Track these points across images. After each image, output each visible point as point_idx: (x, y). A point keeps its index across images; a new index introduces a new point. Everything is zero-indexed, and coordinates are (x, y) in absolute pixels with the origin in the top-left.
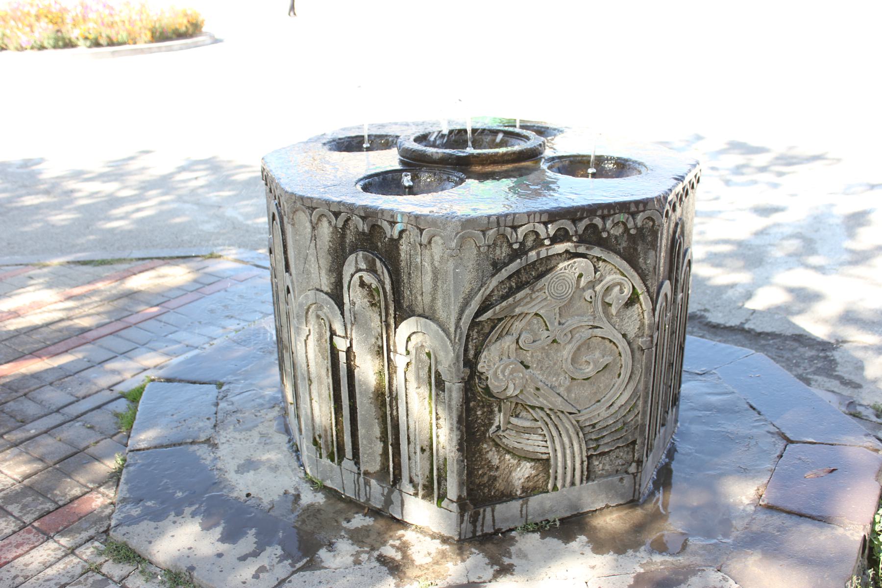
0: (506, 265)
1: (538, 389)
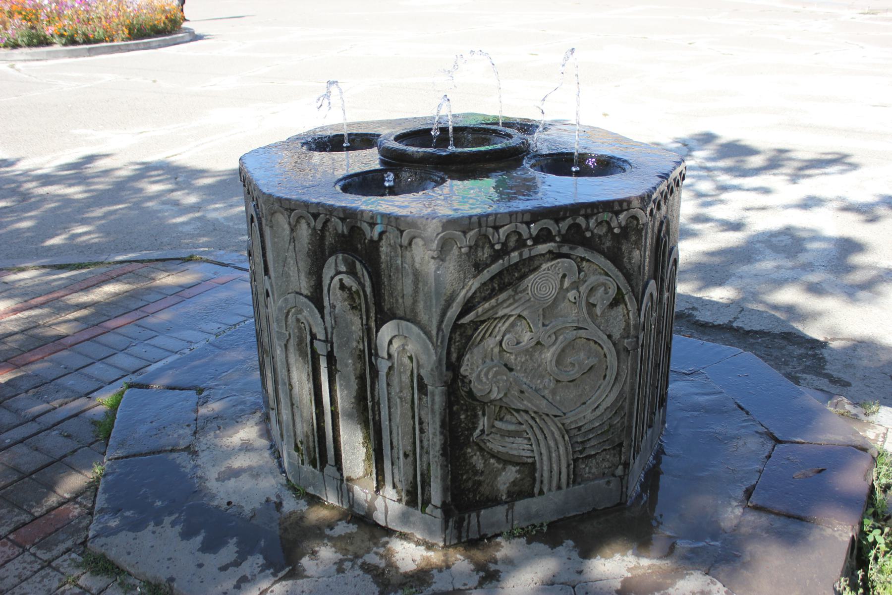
0: (488, 266)
1: (522, 392)
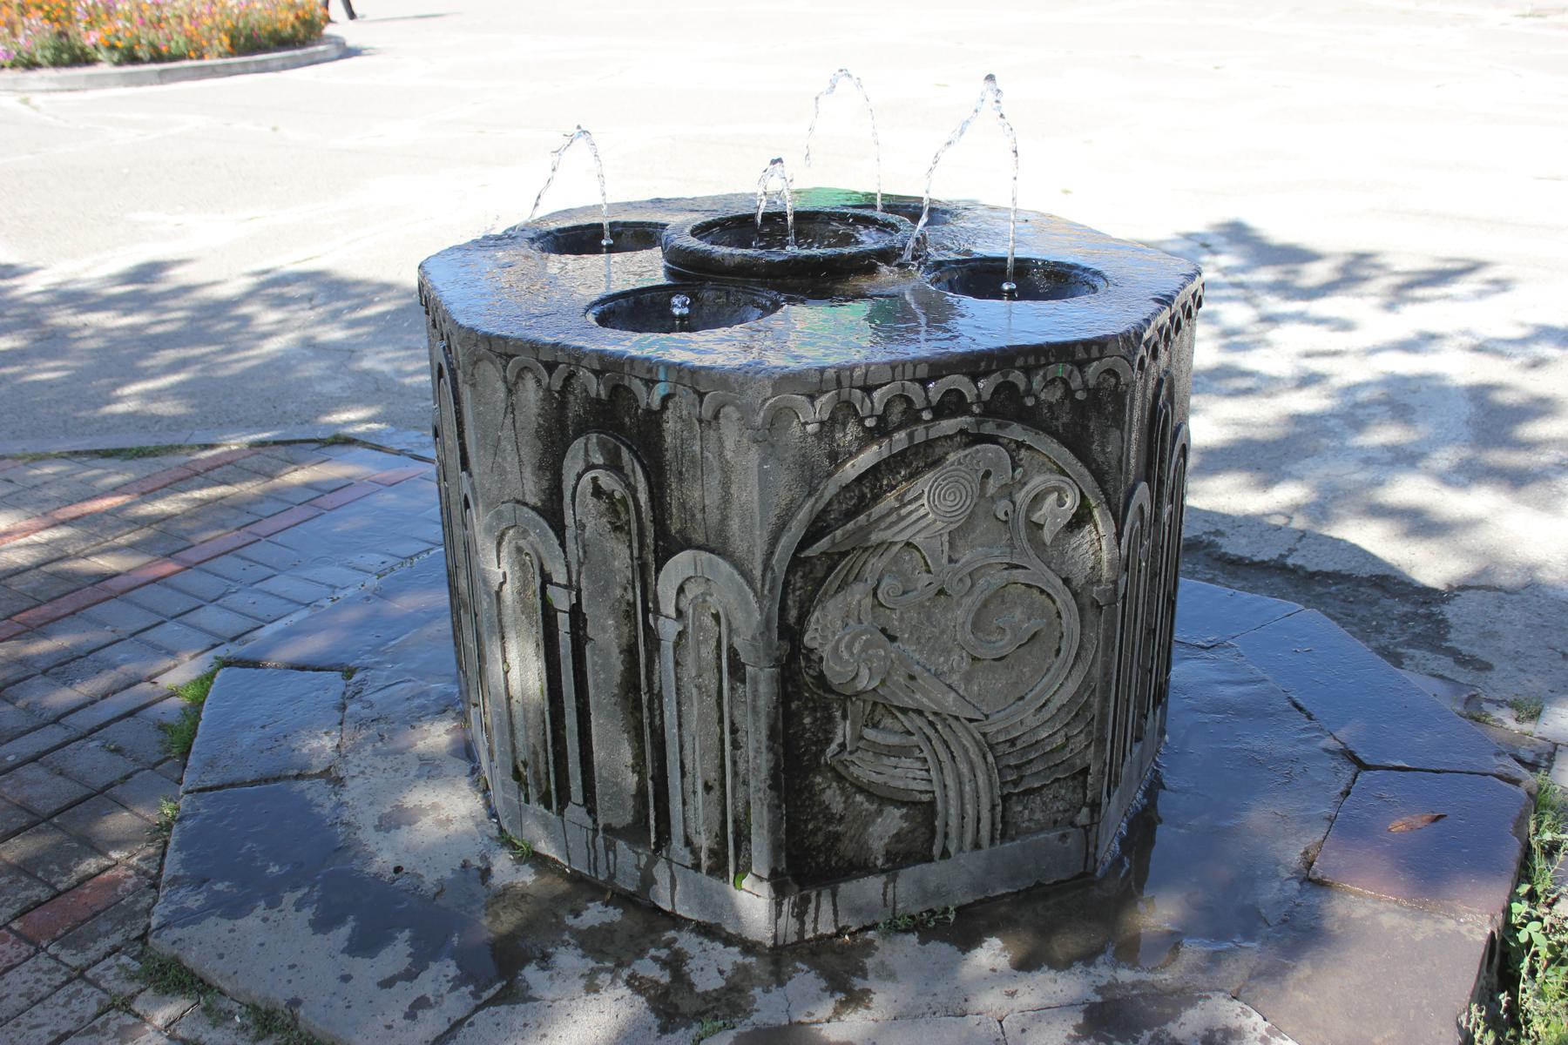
1: (912, 678)
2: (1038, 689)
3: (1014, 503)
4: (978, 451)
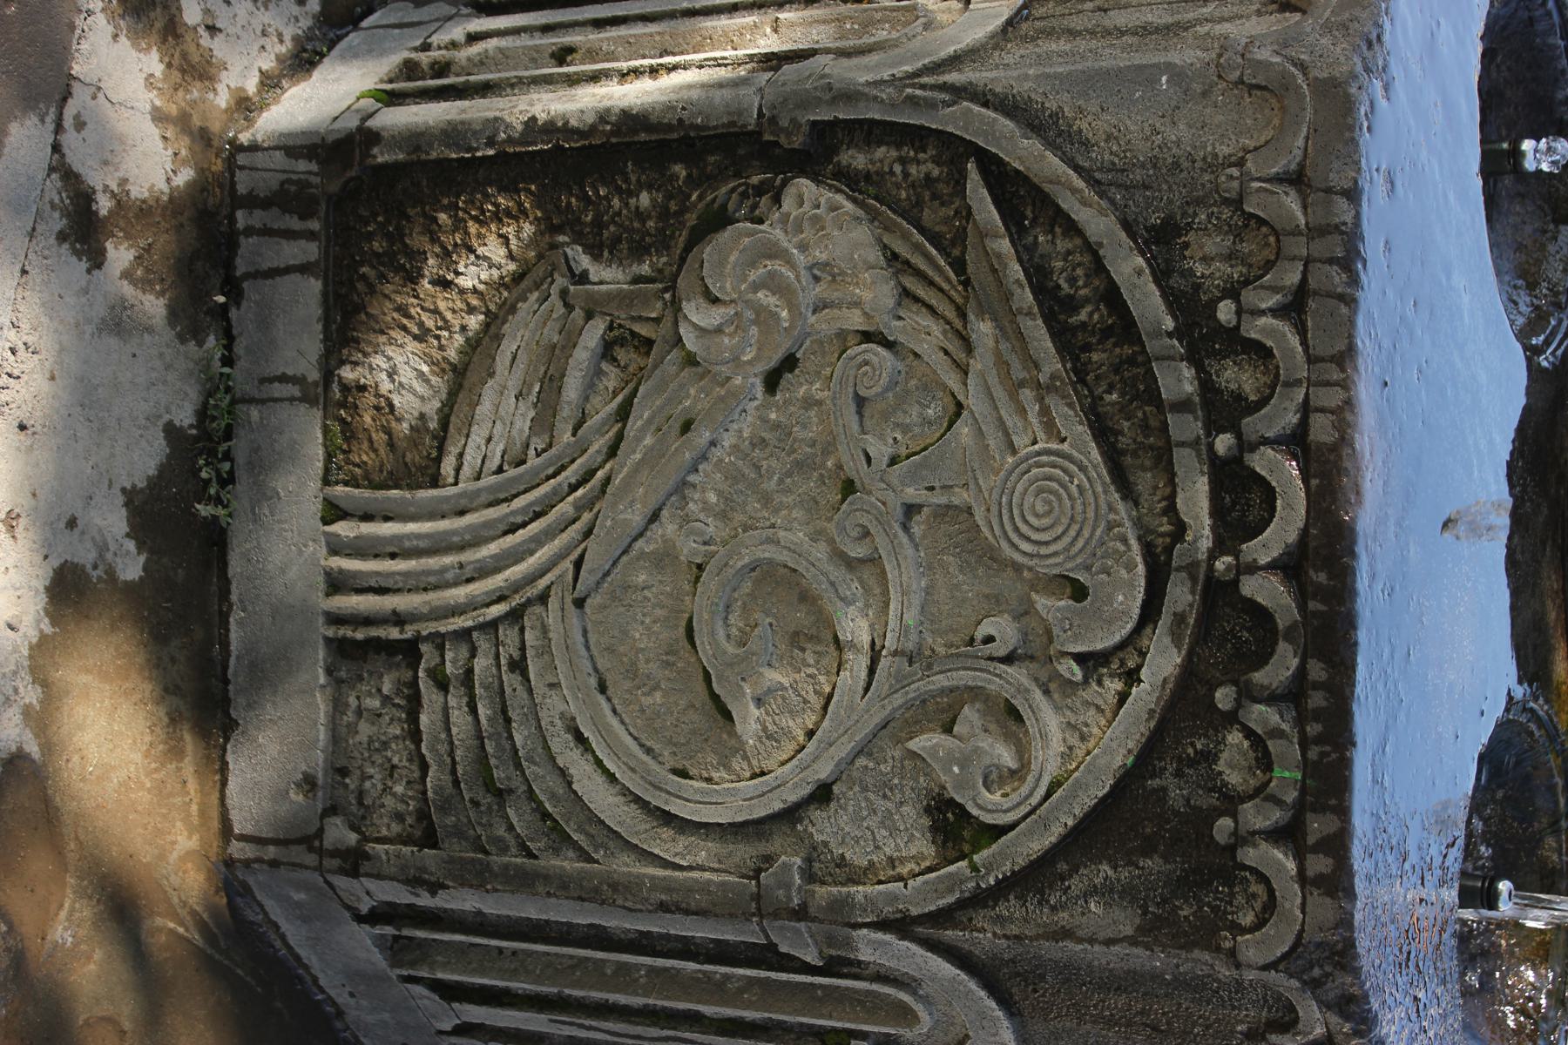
0: (1161, 276)
1: (686, 427)
2: (614, 722)
3: (1009, 659)
4: (1130, 567)
